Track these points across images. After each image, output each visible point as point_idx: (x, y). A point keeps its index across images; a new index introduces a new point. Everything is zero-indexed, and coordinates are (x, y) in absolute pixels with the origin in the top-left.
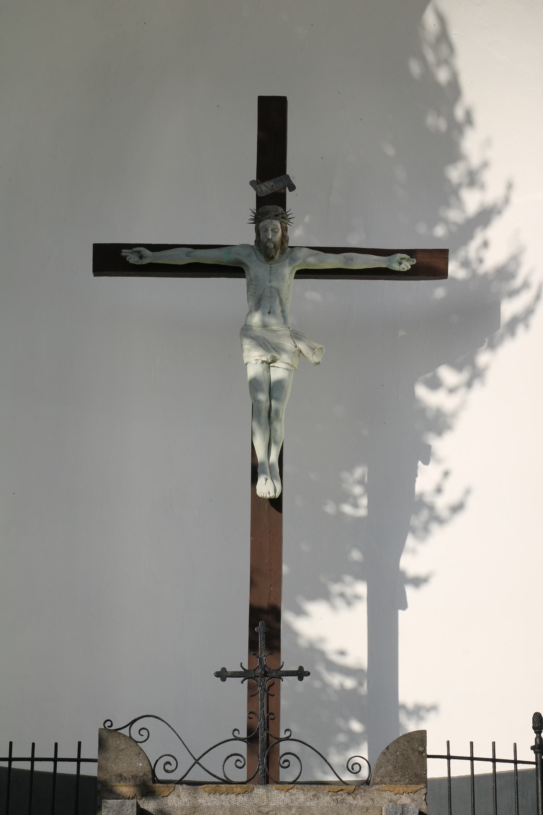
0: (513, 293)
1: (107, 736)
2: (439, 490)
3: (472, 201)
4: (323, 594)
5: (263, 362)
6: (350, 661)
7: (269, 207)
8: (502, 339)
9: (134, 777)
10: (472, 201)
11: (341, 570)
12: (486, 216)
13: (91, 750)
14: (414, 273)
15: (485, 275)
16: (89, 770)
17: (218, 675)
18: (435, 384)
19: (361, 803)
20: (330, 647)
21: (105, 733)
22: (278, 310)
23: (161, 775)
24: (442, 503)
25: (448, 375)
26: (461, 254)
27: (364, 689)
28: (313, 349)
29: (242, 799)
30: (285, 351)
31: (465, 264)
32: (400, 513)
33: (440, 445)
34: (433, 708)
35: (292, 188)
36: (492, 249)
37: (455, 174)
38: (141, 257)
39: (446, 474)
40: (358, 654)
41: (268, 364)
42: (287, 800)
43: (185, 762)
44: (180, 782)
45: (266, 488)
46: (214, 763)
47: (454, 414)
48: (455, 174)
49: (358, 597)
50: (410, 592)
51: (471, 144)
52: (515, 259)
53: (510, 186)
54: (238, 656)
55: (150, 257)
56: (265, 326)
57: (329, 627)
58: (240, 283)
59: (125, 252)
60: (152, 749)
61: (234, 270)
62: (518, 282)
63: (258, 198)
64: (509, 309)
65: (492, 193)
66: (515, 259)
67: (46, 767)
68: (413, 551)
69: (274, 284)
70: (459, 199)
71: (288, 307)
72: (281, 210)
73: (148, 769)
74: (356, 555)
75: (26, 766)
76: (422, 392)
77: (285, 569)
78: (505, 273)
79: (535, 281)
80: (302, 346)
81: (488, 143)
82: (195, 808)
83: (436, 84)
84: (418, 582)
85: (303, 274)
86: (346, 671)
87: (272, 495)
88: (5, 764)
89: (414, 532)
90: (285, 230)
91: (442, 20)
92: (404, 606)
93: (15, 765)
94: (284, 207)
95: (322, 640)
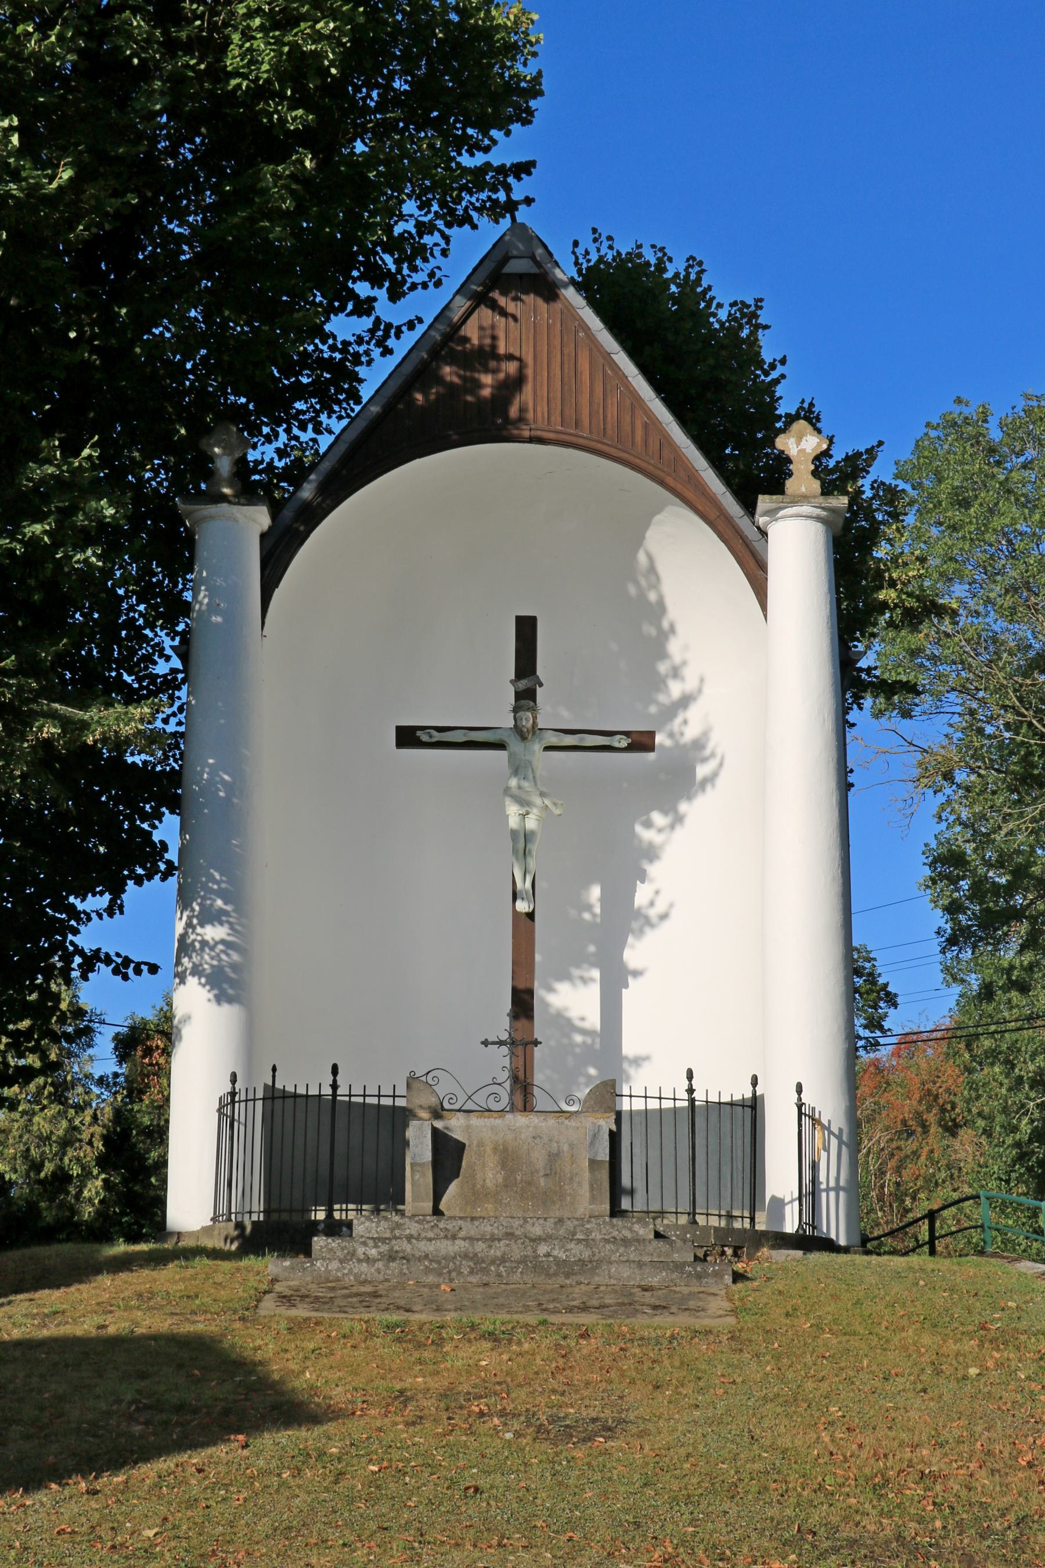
0: (704, 760)
1: (412, 1081)
2: (652, 904)
3: (676, 689)
4: (565, 976)
5: (904, 1122)
6: (586, 1025)
7: (523, 702)
8: (695, 795)
9: (430, 1107)
10: (676, 689)
11: (581, 960)
12: (685, 701)
13: (401, 1090)
14: (630, 748)
15: (685, 745)
16: (401, 1102)
17: (482, 1043)
18: (648, 824)
19: (574, 1124)
20: (574, 1014)
21: (410, 1080)
22: (531, 776)
23: (446, 1106)
24: (653, 913)
25: (658, 818)
26: (668, 727)
27: (598, 1046)
28: (555, 804)
29: (499, 1121)
30: (535, 806)
31: (671, 735)
32: (623, 920)
33: (653, 870)
34: (647, 1058)
35: (541, 685)
36: (691, 725)
37: (663, 668)
38: (431, 737)
39: (657, 892)
40: (593, 1020)
41: (523, 816)
42: (527, 1122)
43: (462, 1098)
44: (459, 1110)
45: (522, 906)
46: (480, 1099)
47: (661, 847)
48: (663, 668)
49: (592, 980)
50: (631, 980)
51: (674, 647)
52: (706, 733)
53: (702, 680)
54: (501, 1026)
55: (437, 736)
56: (520, 787)
57: (572, 999)
58: (502, 754)
59: (419, 733)
60: (441, 1090)
61: (500, 746)
62: (707, 752)
63: (516, 692)
64: (702, 771)
65: (690, 684)
66: (706, 733)
67: (374, 1101)
68: (632, 947)
69: (528, 757)
70: (666, 686)
71: (538, 774)
72: (532, 704)
73: (438, 1102)
74: (592, 949)
75: (360, 1100)
76: (639, 829)
77: (538, 957)
78: (698, 745)
79: (719, 752)
80: (547, 802)
81: (686, 647)
82: (468, 1127)
83: (648, 603)
84: (636, 974)
85: (548, 748)
86: (584, 1032)
87: (527, 910)
88: (347, 1099)
89: (633, 933)
90: (535, 718)
91: (650, 558)
92: (627, 986)
93: (353, 1099)
94: (535, 701)
95: (566, 1009)
